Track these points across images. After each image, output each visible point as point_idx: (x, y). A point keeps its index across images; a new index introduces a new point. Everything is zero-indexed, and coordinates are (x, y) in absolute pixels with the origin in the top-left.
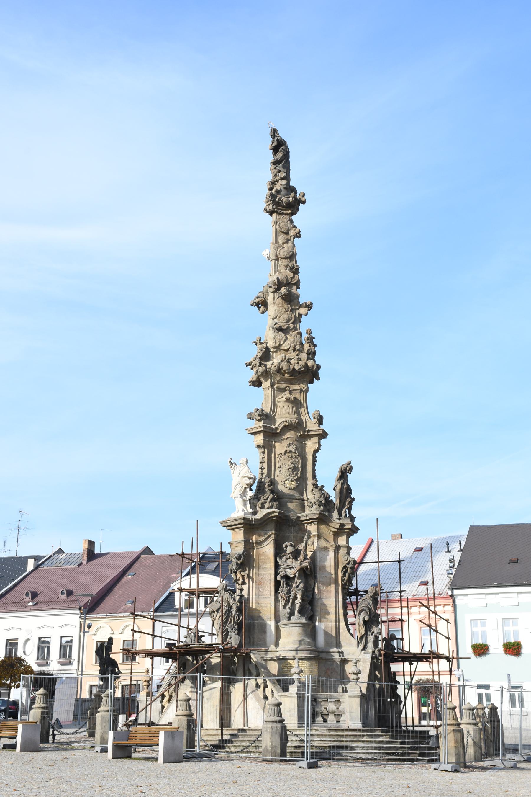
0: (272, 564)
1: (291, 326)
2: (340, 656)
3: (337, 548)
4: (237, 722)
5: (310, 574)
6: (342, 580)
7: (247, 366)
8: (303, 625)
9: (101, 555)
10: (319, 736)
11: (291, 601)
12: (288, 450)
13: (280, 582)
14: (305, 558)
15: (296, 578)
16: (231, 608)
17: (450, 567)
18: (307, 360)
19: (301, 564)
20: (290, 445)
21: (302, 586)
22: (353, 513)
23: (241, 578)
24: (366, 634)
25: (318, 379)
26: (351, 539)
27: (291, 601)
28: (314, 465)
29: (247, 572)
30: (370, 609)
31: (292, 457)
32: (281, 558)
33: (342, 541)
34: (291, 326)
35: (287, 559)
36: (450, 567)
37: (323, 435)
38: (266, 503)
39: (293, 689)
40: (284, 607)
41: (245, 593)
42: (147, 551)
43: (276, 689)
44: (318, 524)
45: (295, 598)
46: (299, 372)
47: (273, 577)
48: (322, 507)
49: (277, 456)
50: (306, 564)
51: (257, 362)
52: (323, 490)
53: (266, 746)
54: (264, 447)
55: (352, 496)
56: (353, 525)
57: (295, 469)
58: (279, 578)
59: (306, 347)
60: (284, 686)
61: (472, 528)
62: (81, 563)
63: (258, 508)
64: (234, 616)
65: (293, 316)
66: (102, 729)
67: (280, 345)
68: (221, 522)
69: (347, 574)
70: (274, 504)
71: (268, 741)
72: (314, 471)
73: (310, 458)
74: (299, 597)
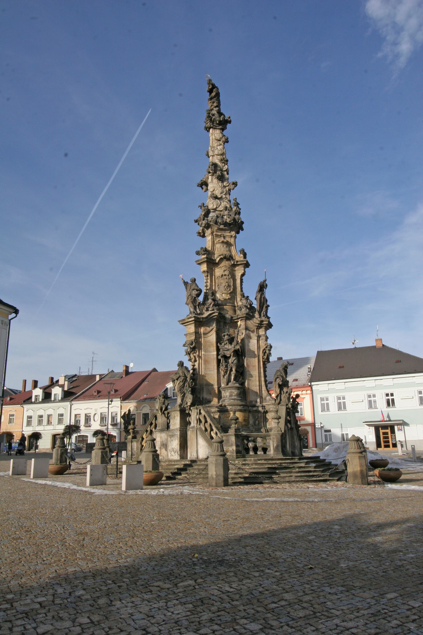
0: (215, 348)
1: (224, 196)
2: (263, 409)
3: (259, 337)
4: (191, 455)
5: (240, 354)
6: (263, 358)
7: (195, 222)
8: (238, 388)
9: (132, 373)
10: (252, 464)
11: (228, 373)
12: (224, 274)
13: (220, 360)
14: (237, 343)
15: (232, 357)
16: (187, 378)
17: (309, 371)
18: (235, 215)
19: (234, 347)
20: (225, 270)
21: (235, 361)
22: (269, 315)
23: (193, 358)
24: (280, 393)
25: (242, 230)
26: (268, 332)
27: (228, 373)
28: (241, 285)
29: (197, 353)
30: (282, 377)
31: (226, 278)
32: (221, 344)
33: (262, 332)
34: (224, 196)
35: (225, 344)
36: (309, 371)
37: (247, 265)
38: (209, 307)
39: (232, 432)
40: (224, 376)
41: (196, 367)
42: (155, 370)
43: (219, 432)
44: (245, 321)
45: (231, 370)
46: (230, 224)
47: (215, 356)
48: (247, 310)
49: (216, 278)
50: (238, 347)
51: (202, 217)
52: (248, 299)
53: (212, 475)
54: (208, 272)
55: (268, 303)
56: (269, 322)
57: (229, 286)
58: (220, 357)
59: (234, 208)
60: (225, 429)
61: (318, 352)
62: (122, 377)
63: (204, 311)
64: (189, 383)
65: (225, 190)
66: (95, 461)
67: (217, 208)
68: (179, 321)
69: (266, 354)
70: (215, 308)
71: (214, 471)
72: (242, 288)
73: (238, 281)
74: (234, 370)
